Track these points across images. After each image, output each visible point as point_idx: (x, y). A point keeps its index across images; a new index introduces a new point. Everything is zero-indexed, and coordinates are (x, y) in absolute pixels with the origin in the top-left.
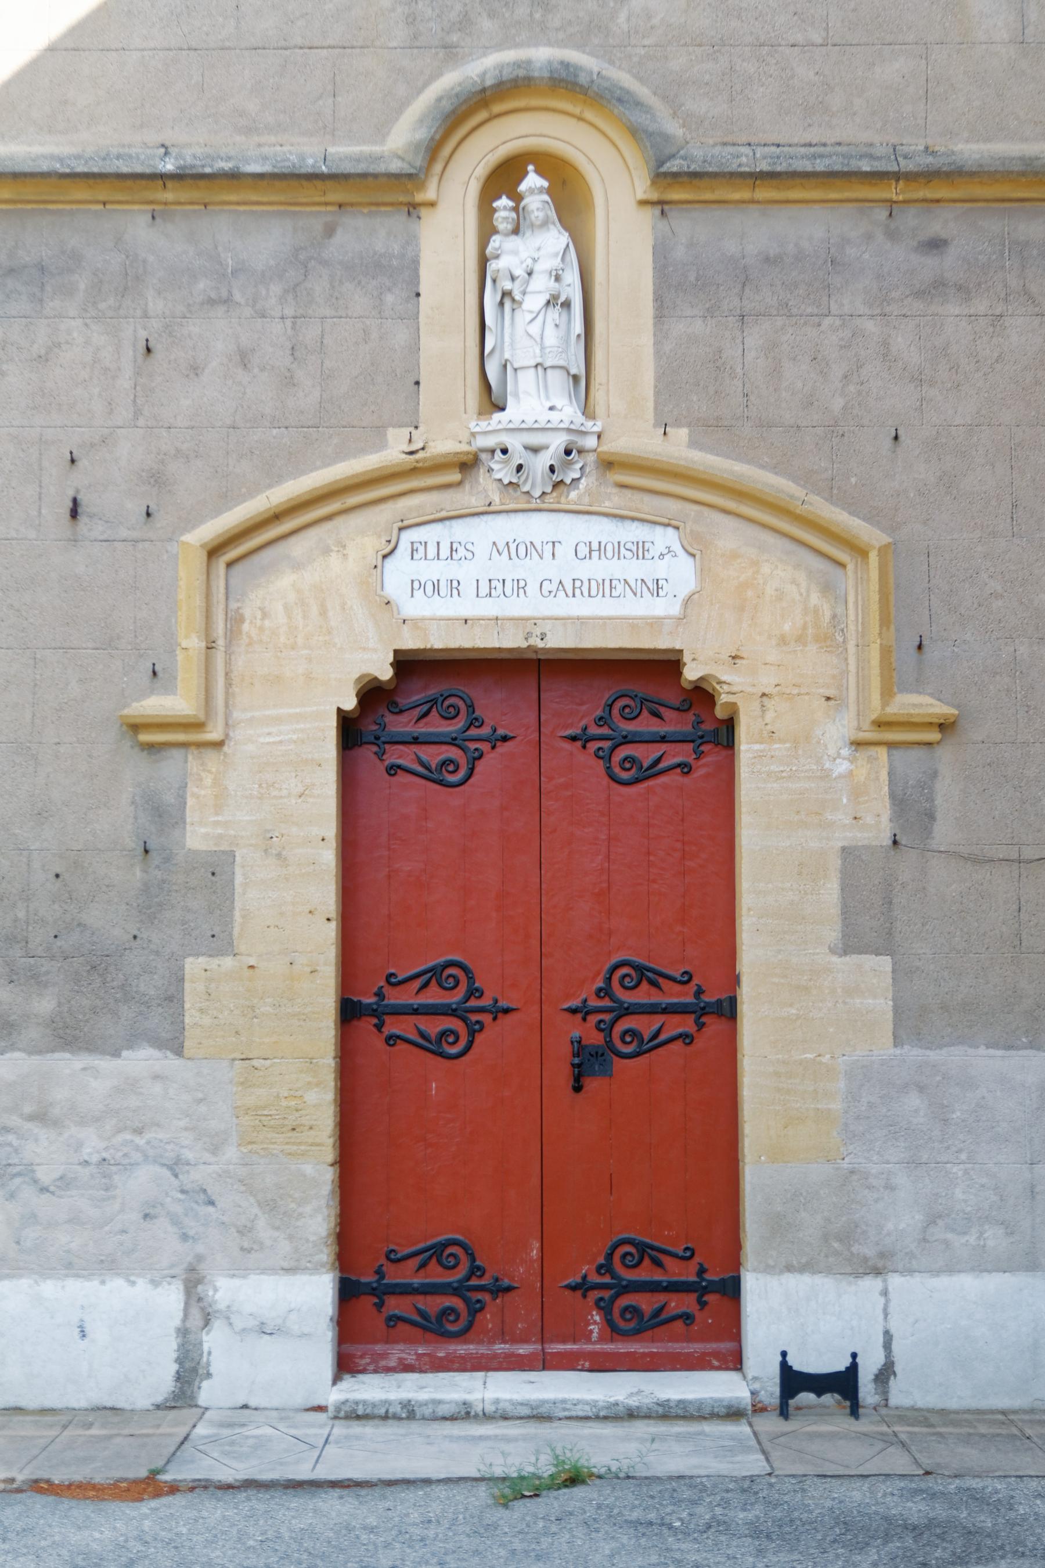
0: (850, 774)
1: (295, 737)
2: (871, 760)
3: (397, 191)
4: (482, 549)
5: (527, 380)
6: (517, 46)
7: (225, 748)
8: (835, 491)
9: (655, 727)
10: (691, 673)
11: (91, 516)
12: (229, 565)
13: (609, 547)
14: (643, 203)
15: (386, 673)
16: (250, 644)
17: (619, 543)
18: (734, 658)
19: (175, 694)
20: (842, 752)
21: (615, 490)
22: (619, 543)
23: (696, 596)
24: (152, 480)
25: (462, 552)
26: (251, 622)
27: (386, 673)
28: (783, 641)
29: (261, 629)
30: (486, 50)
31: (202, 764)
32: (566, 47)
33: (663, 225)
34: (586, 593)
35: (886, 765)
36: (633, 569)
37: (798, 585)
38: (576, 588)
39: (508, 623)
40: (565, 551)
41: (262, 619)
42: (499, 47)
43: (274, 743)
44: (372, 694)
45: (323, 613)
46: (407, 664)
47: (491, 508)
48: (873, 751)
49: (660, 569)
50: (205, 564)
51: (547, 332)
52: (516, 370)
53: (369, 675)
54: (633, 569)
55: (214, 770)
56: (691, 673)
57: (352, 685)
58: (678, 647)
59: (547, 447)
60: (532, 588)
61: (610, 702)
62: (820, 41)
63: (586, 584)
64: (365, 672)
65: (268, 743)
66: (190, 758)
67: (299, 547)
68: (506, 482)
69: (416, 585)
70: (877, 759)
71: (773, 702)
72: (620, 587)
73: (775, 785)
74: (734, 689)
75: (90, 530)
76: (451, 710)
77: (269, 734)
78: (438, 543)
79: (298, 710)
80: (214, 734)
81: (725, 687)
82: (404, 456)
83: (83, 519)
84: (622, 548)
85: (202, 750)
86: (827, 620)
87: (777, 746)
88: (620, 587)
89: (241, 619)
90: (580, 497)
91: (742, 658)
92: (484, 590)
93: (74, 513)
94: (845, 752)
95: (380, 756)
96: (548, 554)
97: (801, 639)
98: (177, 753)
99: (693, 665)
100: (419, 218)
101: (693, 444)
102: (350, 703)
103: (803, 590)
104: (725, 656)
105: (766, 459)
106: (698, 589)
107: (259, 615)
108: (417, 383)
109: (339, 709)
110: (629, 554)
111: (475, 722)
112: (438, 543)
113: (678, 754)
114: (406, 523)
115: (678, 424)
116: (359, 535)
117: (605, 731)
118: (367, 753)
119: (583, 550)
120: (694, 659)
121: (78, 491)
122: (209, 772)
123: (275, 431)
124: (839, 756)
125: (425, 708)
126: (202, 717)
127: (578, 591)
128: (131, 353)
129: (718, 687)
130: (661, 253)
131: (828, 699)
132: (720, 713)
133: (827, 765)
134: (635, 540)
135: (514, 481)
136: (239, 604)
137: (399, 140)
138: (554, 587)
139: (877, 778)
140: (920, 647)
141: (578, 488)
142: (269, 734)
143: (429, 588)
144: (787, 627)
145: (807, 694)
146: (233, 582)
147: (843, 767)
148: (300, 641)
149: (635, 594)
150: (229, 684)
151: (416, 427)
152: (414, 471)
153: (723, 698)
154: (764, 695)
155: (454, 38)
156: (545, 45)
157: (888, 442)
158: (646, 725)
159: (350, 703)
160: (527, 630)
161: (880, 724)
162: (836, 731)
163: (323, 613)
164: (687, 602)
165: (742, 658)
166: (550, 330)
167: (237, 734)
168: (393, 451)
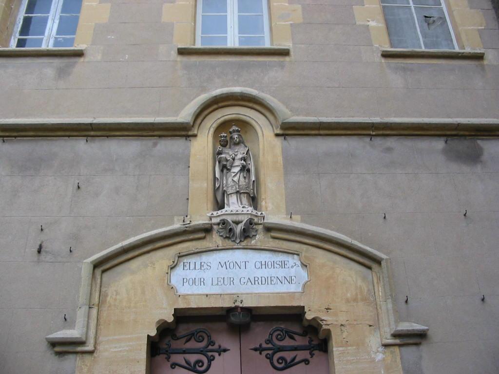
0: (384, 360)
1: (127, 349)
2: (392, 353)
3: (182, 131)
4: (214, 265)
5: (233, 199)
6: (227, 87)
7: (95, 354)
8: (363, 239)
9: (292, 343)
10: (309, 316)
11: (46, 252)
12: (104, 271)
13: (270, 263)
14: (277, 135)
15: (170, 319)
16: (109, 306)
17: (274, 262)
18: (327, 309)
19: (74, 329)
20: (379, 349)
21: (271, 240)
22: (274, 262)
23: (309, 283)
24: (74, 238)
25: (205, 267)
26: (111, 297)
27: (170, 319)
28: (348, 301)
29: (115, 300)
30: (217, 88)
31: (83, 362)
32: (246, 87)
33: (285, 143)
34: (260, 283)
35: (399, 354)
36: (281, 273)
37: (352, 277)
38: (255, 281)
39: (226, 297)
40: (250, 266)
41: (116, 295)
42: (222, 87)
43: (117, 351)
44: (165, 330)
45: (143, 293)
46: (183, 316)
47: (219, 248)
48: (392, 349)
49: (293, 272)
50: (91, 272)
51: (241, 179)
52: (228, 195)
53: (163, 320)
54: (281, 273)
55: (88, 365)
56: (309, 316)
57: (155, 324)
58: (302, 305)
59: (242, 222)
60: (236, 281)
61: (271, 333)
62: (337, 86)
63: (260, 279)
64: (161, 318)
65: (115, 352)
66: (78, 358)
67: (134, 264)
68: (224, 236)
69: (185, 280)
70: (394, 352)
71: (346, 328)
72: (275, 280)
73: (350, 366)
74: (328, 323)
75: (45, 258)
76: (201, 338)
77: (115, 347)
78: (195, 263)
79: (129, 336)
80: (89, 347)
81: (324, 322)
82: (182, 226)
83: (43, 253)
84: (275, 264)
85: (84, 355)
86: (366, 291)
87: (349, 348)
88: (275, 280)
89: (106, 296)
90: (256, 243)
91: (331, 309)
92: (215, 282)
93: (39, 252)
94: (381, 349)
95: (168, 359)
96: (243, 267)
97: (355, 300)
98: (71, 357)
99: (309, 312)
100: (190, 140)
101: (303, 221)
102: (153, 333)
103: (354, 280)
104: (323, 308)
105: (333, 227)
106: (309, 280)
107: (115, 293)
108: (188, 199)
109: (148, 336)
110: (278, 266)
111: (212, 343)
112: (195, 263)
113: (301, 355)
114: (181, 254)
115: (296, 214)
116: (162, 258)
117: (270, 346)
118: (161, 358)
119: (258, 265)
120: (309, 310)
121: (42, 242)
122: (86, 365)
123: (128, 218)
124: (378, 352)
125: (189, 337)
126: (84, 339)
127: (256, 282)
128: (72, 188)
129: (321, 322)
130: (284, 152)
131: (370, 326)
132: (321, 336)
133: (373, 356)
134: (281, 260)
135: (228, 236)
136: (106, 289)
137: (185, 115)
138: (246, 280)
139: (396, 361)
140: (406, 302)
141: (255, 239)
142: (115, 347)
143: (191, 282)
144: (349, 295)
145: (361, 324)
146: (104, 279)
147: (380, 356)
148: (132, 305)
149: (282, 283)
150: (98, 325)
151: (187, 216)
152: (184, 232)
153: (324, 327)
154: (342, 325)
155: (205, 84)
156: (238, 86)
157: (382, 220)
158: (287, 342)
159: (153, 333)
160: (235, 299)
161: (395, 336)
162: (374, 341)
163: (143, 293)
164: (304, 286)
165: (331, 309)
166: (242, 179)
167: (100, 348)
168: (177, 225)
